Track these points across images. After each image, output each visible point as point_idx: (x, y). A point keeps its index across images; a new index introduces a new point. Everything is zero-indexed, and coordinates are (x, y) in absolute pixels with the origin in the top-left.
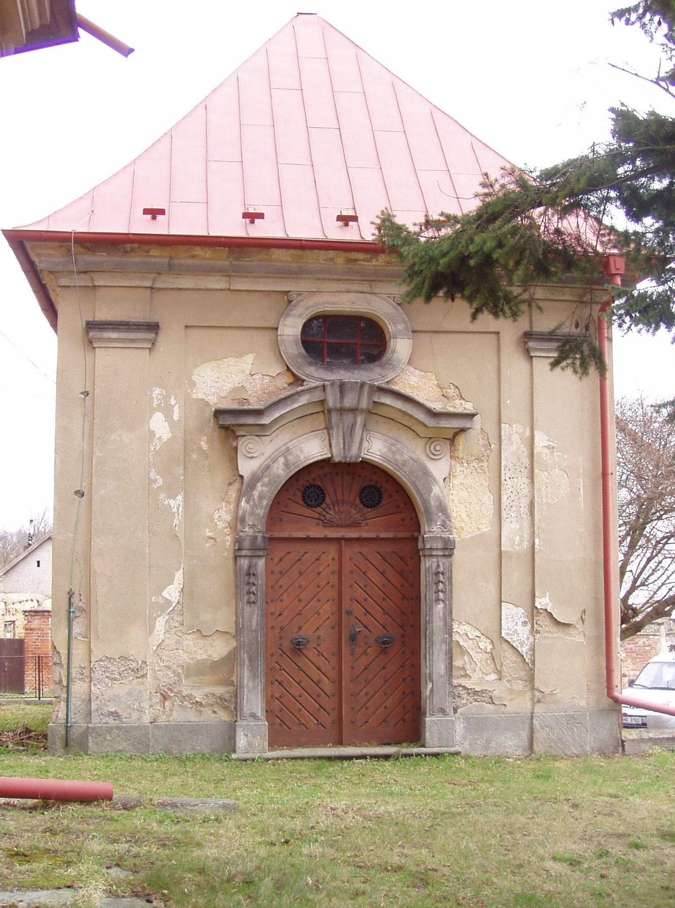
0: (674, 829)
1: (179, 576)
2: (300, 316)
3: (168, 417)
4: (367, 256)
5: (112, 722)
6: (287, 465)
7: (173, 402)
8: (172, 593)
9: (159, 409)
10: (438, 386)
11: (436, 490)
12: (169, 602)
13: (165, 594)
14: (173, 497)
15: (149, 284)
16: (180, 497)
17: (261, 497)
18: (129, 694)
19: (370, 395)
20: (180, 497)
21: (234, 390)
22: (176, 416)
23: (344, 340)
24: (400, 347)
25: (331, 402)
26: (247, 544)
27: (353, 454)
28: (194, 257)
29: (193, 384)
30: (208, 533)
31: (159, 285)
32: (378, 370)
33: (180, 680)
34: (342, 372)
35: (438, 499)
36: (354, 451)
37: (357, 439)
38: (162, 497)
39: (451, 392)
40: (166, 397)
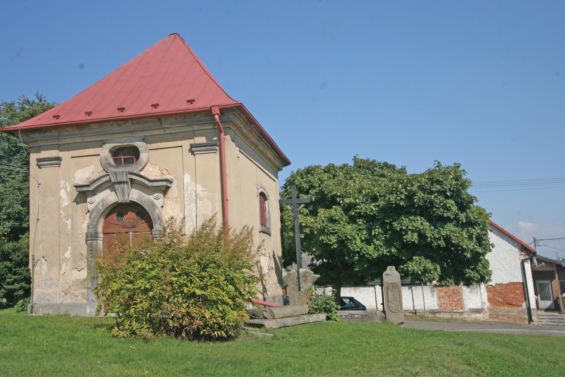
0: (564, 265)
1: (70, 248)
2: (106, 149)
3: (66, 191)
4: (124, 122)
5: (47, 302)
6: (103, 205)
7: (67, 185)
8: (68, 255)
9: (63, 188)
10: (160, 170)
11: (157, 211)
12: (66, 258)
13: (65, 255)
14: (68, 219)
15: (56, 143)
16: (70, 220)
17: (94, 218)
18: (53, 292)
19: (126, 176)
20: (70, 220)
21: (87, 179)
22: (69, 190)
23: (127, 155)
24: (143, 156)
25: (113, 180)
26: (89, 235)
27: (127, 199)
28: (66, 131)
29: (74, 178)
30: (80, 232)
31: (61, 143)
32: (135, 166)
33: (70, 287)
34: (122, 168)
35: (158, 215)
36: (126, 198)
37: (127, 194)
38: (64, 219)
39: (165, 172)
40: (65, 184)
